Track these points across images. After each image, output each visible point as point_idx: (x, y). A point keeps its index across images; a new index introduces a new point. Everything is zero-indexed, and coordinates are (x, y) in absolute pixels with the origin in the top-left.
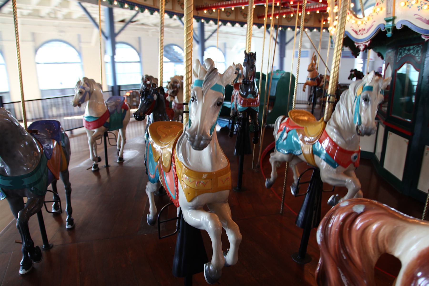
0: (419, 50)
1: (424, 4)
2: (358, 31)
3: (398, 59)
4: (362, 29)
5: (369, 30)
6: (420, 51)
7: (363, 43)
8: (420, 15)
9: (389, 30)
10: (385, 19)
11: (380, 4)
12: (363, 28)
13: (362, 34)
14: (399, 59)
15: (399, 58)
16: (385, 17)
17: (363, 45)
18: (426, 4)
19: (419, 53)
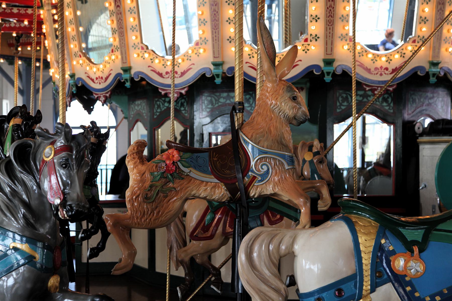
0: (184, 102)
1: (155, 58)
2: (95, 80)
3: (155, 114)
4: (99, 77)
5: (107, 78)
6: (185, 104)
7: (102, 94)
8: (155, 68)
9: (218, 76)
10: (212, 62)
11: (115, 51)
12: (100, 77)
13: (100, 83)
14: (158, 114)
15: (157, 112)
16: (121, 66)
17: (104, 96)
18: (157, 58)
19: (185, 106)
